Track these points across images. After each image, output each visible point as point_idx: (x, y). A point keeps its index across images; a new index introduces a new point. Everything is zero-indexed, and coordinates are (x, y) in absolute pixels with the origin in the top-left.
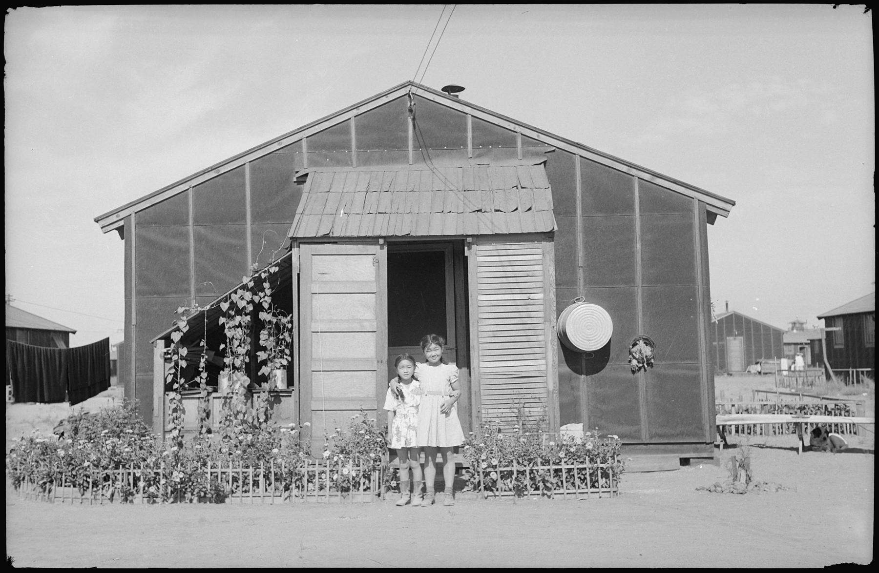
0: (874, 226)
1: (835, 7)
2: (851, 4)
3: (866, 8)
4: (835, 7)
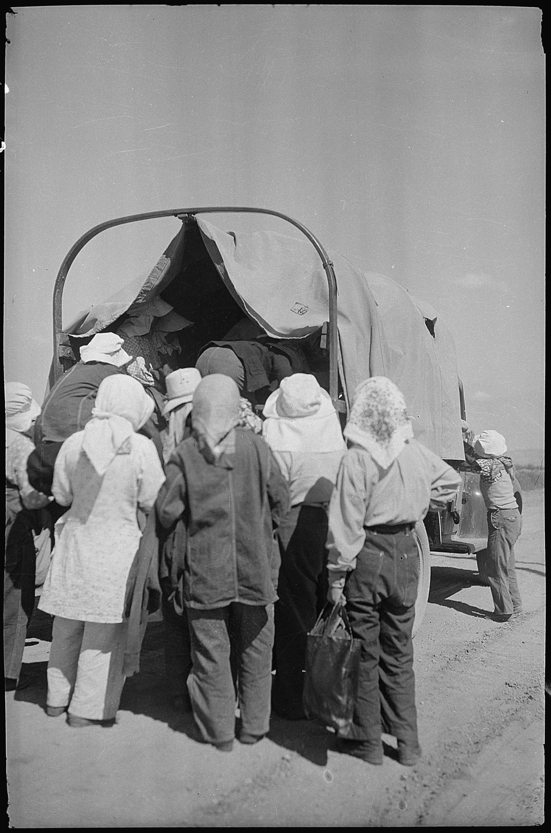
0: (219, 5)
1: (9, 42)
2: (542, 23)
3: (10, 12)
4: (9, 42)
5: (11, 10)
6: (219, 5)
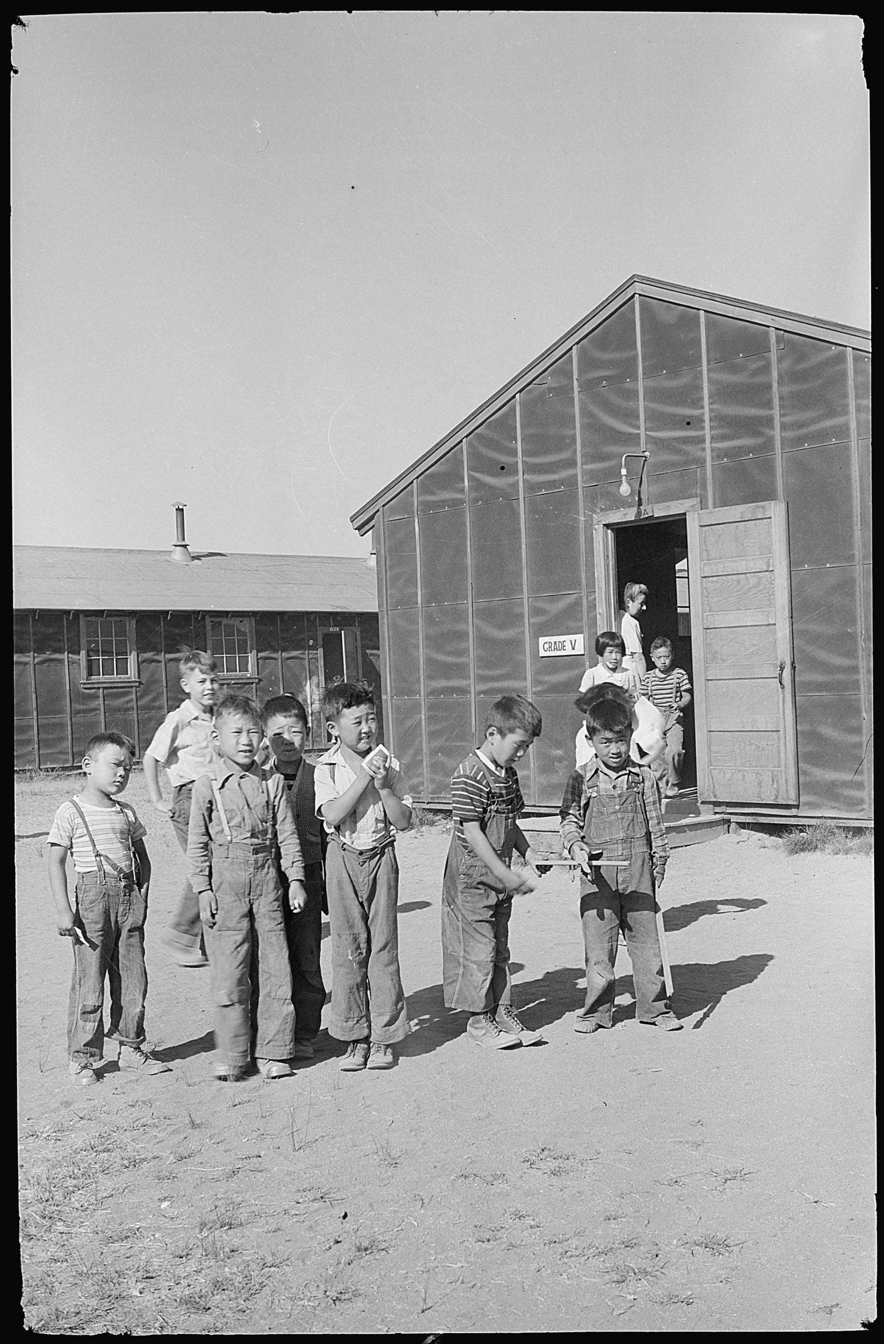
0: (350, 12)
1: (16, 72)
2: (11, 47)
4: (16, 72)
5: (20, 20)
6: (350, 12)
